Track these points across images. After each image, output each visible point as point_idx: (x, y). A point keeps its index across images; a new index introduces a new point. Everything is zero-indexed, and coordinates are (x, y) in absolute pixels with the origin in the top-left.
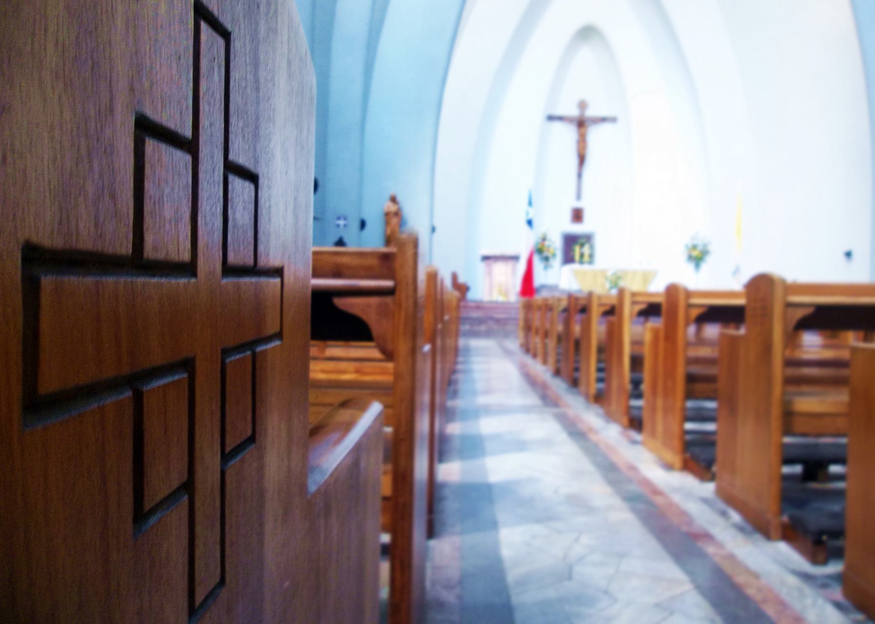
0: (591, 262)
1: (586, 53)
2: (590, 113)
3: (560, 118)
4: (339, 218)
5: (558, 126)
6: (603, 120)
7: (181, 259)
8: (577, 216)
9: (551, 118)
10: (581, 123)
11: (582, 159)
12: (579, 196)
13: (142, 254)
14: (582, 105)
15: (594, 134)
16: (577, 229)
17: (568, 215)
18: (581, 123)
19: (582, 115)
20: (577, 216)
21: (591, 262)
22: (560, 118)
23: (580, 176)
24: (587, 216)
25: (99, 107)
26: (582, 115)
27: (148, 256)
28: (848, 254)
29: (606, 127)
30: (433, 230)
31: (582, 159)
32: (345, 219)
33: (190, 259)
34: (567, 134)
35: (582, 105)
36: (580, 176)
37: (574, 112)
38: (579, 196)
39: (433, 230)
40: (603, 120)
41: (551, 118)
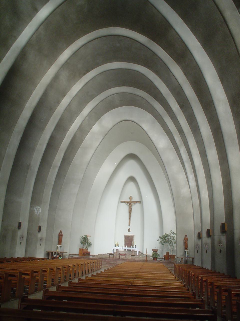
3: (124, 202)
14: (131, 198)
18: (130, 204)
19: (131, 201)
22: (124, 202)
23: (130, 219)
34: (125, 207)
35: (131, 198)
36: (130, 219)
40: (137, 202)
41: (122, 202)
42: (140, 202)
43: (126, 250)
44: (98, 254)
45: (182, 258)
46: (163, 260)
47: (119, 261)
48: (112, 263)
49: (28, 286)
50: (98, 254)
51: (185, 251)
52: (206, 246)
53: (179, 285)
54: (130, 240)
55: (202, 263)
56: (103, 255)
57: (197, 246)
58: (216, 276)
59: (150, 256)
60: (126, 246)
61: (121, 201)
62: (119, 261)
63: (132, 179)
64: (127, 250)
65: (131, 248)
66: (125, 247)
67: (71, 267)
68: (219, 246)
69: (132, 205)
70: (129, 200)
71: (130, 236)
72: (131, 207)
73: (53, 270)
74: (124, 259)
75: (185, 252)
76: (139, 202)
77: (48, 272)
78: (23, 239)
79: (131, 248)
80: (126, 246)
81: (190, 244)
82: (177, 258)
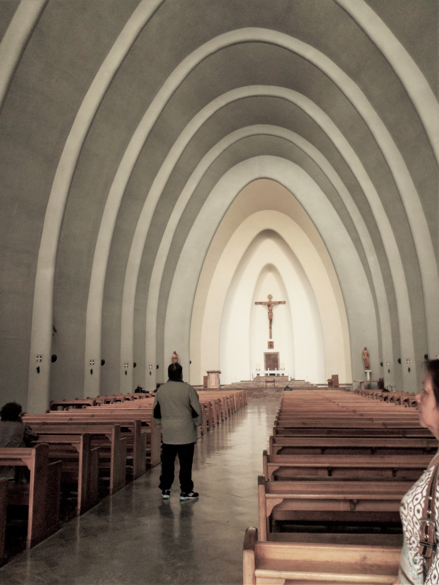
1: (270, 275)
2: (273, 300)
3: (261, 303)
4: (150, 366)
5: (260, 306)
6: (280, 303)
7: (215, 374)
8: (271, 345)
9: (256, 303)
10: (270, 305)
11: (271, 321)
12: (271, 337)
13: (338, 383)
14: (270, 297)
15: (277, 310)
17: (267, 345)
18: (270, 305)
19: (270, 301)
20: (271, 345)
22: (261, 303)
23: (270, 328)
25: (427, 480)
26: (270, 301)
27: (259, 413)
28: (236, 378)
29: (281, 306)
31: (271, 321)
32: (152, 366)
33: (204, 384)
34: (263, 311)
35: (270, 297)
36: (270, 328)
37: (267, 300)
38: (271, 337)
39: (190, 362)
41: (256, 303)
44: (232, 383)
45: (363, 382)
46: (327, 387)
48: (256, 393)
50: (232, 383)
51: (366, 371)
52: (408, 362)
53: (415, 412)
55: (159, 464)
56: (238, 384)
58: (375, 422)
59: (368, 371)
60: (268, 369)
62: (266, 391)
63: (270, 268)
65: (275, 372)
67: (148, 425)
69: (272, 308)
71: (272, 354)
72: (271, 310)
73: (130, 431)
75: (366, 373)
77: (112, 439)
79: (275, 372)
80: (268, 369)
81: (374, 361)
82: (354, 383)
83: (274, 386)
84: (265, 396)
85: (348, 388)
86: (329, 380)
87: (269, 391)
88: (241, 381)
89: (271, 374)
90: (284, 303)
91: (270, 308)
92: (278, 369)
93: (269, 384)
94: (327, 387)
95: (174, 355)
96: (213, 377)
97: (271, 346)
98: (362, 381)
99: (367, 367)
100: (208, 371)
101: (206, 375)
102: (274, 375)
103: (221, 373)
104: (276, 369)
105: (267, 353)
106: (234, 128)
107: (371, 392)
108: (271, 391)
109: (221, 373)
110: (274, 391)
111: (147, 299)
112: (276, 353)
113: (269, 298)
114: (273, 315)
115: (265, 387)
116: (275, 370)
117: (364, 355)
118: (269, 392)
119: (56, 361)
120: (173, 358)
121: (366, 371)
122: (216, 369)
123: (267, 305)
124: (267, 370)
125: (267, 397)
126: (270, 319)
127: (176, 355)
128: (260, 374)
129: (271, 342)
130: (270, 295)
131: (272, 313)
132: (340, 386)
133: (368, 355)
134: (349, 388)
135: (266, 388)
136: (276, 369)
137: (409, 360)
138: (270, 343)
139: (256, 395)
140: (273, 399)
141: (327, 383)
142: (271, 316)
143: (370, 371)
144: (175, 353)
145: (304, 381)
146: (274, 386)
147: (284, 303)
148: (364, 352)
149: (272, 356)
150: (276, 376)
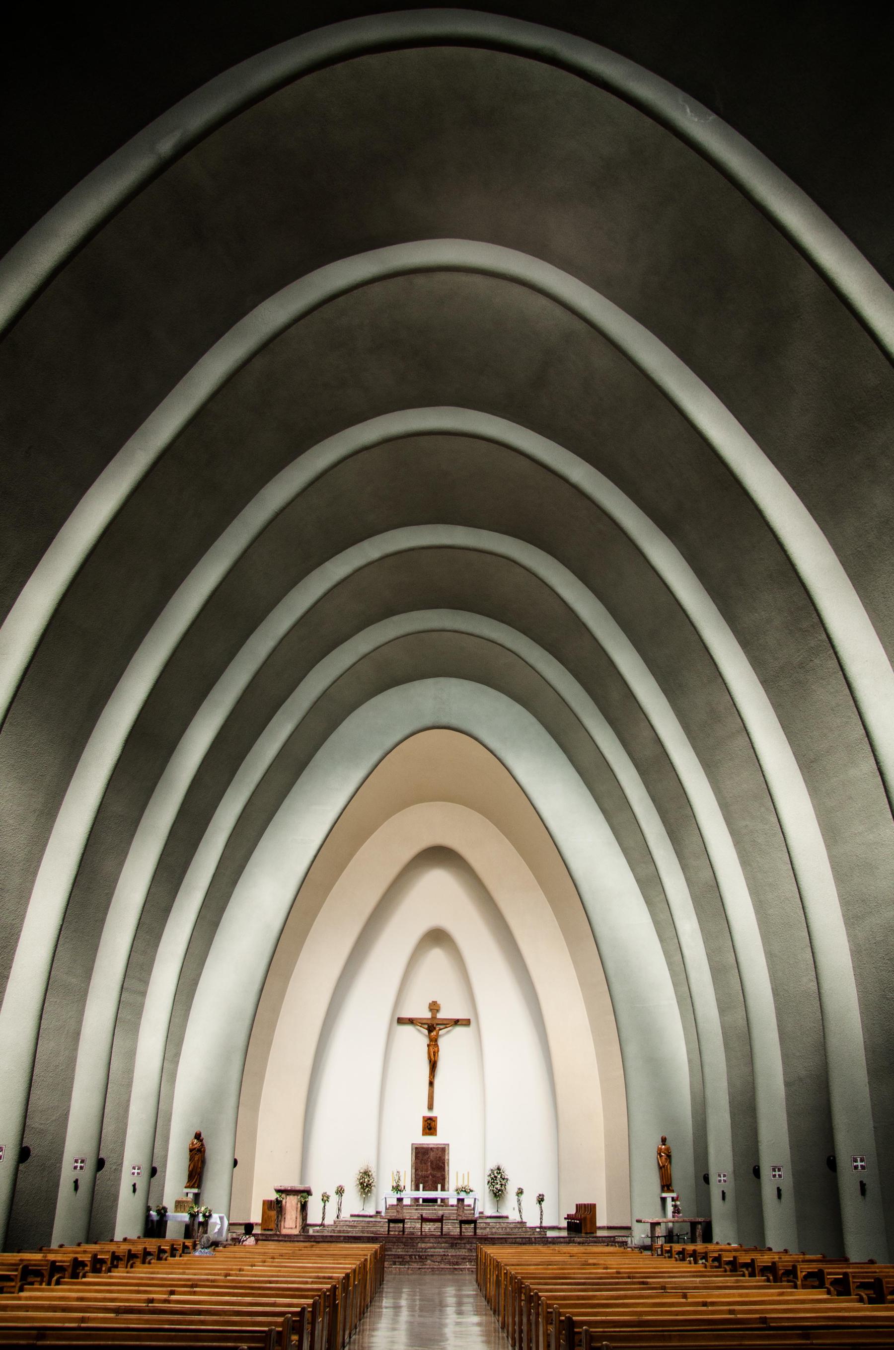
0: (448, 1191)
1: (437, 956)
3: (411, 1021)
5: (409, 1029)
6: (456, 1022)
8: (430, 1126)
9: (401, 1021)
11: (433, 1066)
12: (430, 1107)
14: (434, 1007)
15: (448, 1040)
16: (429, 1141)
18: (431, 1029)
20: (430, 1126)
21: (448, 1191)
22: (411, 1021)
23: (431, 1084)
24: (440, 1126)
29: (459, 1030)
30: (235, 1163)
31: (433, 1066)
34: (417, 1039)
35: (434, 1007)
36: (431, 1084)
38: (430, 1107)
39: (235, 1163)
40: (456, 1022)
41: (401, 1021)
42: (469, 1020)
43: (421, 1200)
45: (659, 1224)
46: (564, 1234)
47: (423, 1245)
48: (400, 1252)
49: (828, 1277)
51: (664, 1195)
52: (777, 1173)
54: (432, 1162)
57: (720, 1176)
59: (668, 1195)
60: (421, 1186)
61: (399, 1019)
62: (423, 1245)
64: (425, 1200)
65: (438, 1194)
66: (413, 1188)
68: (774, 1176)
70: (428, 1015)
71: (431, 1149)
72: (436, 1040)
74: (443, 1236)
75: (663, 1200)
76: (464, 1022)
78: (83, 1157)
79: (438, 1194)
80: (421, 1186)
83: (442, 1232)
84: (422, 1259)
85: (620, 1239)
86: (569, 1217)
87: (431, 1245)
88: (352, 1216)
89: (426, 1200)
90: (467, 1023)
91: (433, 1034)
92: (443, 1189)
93: (428, 1227)
94: (564, 1234)
95: (196, 1141)
96: (291, 1203)
97: (430, 1129)
98: (655, 1220)
99: (666, 1186)
100: (280, 1188)
101: (274, 1196)
102: (434, 1200)
103: (311, 1195)
104: (439, 1186)
105: (419, 1146)
106: (388, 612)
107: (677, 1247)
108: (435, 1245)
109: (311, 1195)
110: (443, 1245)
111: (144, 994)
112: (443, 1146)
113: (431, 1010)
114: (438, 1051)
115: (420, 1233)
116: (436, 1190)
117: (661, 1156)
118: (431, 1248)
119: (29, 1160)
120: (191, 1150)
121: (664, 1195)
122: (297, 1186)
123: (426, 1026)
124: (417, 1189)
125: (429, 1261)
126: (430, 1062)
127: (201, 1141)
128: (404, 1200)
129: (430, 1119)
130: (433, 1002)
131: (437, 1045)
132: (600, 1233)
133: (669, 1156)
134: (624, 1239)
135: (423, 1237)
136: (439, 1186)
137: (779, 1170)
138: (429, 1121)
139: (399, 1256)
140: (442, 1266)
141: (564, 1224)
142: (434, 1055)
143: (674, 1195)
144: (198, 1136)
145: (507, 1217)
146: (442, 1232)
147: (467, 1023)
148: (661, 1149)
149: (432, 1155)
150: (439, 1206)
